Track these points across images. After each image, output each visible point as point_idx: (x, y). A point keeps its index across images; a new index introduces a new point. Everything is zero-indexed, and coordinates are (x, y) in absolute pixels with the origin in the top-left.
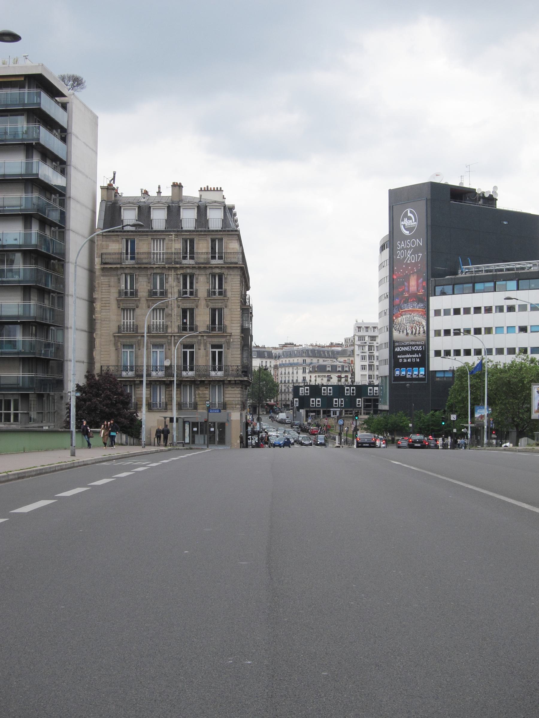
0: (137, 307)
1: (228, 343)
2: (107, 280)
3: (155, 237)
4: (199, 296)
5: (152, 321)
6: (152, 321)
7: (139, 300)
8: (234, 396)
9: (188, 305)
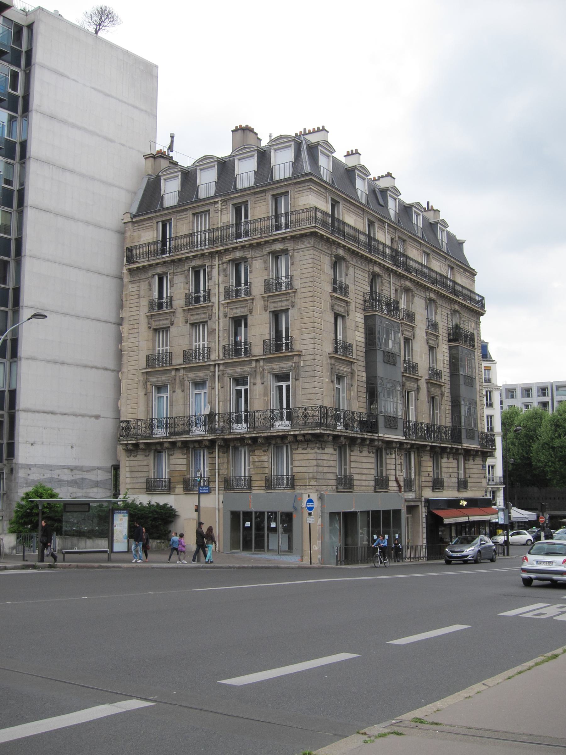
0: (172, 324)
1: (297, 368)
2: (136, 289)
3: (197, 211)
4: (253, 294)
5: (157, 349)
6: (202, 343)
7: (174, 312)
8: (139, 469)
9: (238, 310)
